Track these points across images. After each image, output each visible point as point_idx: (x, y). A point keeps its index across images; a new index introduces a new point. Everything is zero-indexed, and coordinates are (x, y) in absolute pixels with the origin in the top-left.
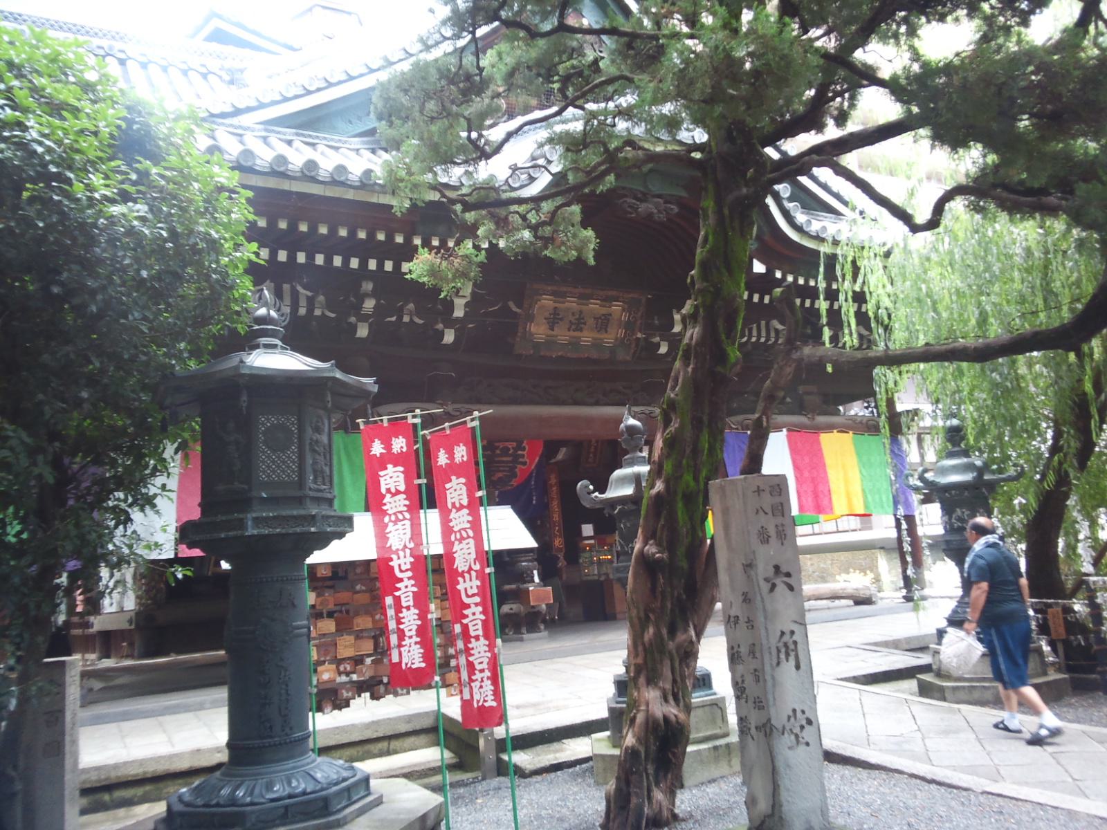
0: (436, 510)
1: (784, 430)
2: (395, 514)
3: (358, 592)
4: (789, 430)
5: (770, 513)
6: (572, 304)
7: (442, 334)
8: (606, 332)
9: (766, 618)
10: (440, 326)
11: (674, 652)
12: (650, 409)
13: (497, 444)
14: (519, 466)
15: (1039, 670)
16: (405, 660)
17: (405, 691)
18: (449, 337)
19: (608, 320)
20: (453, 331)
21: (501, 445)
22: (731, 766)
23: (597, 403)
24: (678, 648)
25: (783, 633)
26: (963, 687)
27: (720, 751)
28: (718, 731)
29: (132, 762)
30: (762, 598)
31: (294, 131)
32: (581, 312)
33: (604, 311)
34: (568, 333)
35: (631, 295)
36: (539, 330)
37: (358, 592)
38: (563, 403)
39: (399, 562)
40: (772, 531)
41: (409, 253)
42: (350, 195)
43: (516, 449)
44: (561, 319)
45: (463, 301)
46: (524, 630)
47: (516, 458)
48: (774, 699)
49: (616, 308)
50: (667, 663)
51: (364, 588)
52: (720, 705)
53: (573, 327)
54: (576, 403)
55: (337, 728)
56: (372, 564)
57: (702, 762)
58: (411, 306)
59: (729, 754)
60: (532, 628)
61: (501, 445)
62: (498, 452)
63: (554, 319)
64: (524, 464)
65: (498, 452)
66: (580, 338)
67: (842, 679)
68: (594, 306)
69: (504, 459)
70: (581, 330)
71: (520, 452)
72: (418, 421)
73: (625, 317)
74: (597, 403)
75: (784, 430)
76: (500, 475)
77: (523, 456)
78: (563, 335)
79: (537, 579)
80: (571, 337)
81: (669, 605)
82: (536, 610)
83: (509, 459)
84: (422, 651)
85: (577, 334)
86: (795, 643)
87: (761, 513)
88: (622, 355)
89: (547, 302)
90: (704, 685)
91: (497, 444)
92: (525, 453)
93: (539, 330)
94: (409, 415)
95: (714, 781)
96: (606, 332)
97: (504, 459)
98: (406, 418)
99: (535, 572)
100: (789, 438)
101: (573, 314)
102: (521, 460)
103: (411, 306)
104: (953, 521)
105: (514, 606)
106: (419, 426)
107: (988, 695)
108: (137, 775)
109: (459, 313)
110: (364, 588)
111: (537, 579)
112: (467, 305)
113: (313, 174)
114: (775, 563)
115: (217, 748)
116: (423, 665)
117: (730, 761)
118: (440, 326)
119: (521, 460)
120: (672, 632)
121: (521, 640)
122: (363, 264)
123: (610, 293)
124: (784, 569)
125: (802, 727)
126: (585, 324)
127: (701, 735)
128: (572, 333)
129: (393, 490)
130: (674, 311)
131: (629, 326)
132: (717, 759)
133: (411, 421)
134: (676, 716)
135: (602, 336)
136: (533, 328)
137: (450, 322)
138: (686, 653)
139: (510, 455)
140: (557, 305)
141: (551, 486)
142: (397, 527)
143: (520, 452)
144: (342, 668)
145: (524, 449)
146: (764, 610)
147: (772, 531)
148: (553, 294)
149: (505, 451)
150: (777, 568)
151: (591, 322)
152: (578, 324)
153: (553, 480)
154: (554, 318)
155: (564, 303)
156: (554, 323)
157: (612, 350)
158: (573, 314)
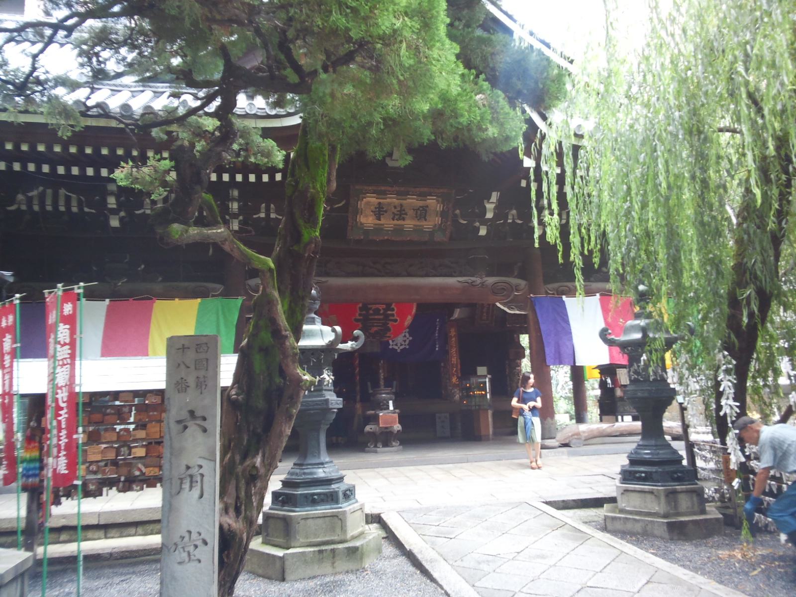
0: (46, 359)
1: (598, 295)
2: (62, 360)
3: (108, 414)
4: (601, 295)
5: (193, 367)
6: (392, 200)
7: (478, 230)
8: (426, 220)
9: (171, 454)
10: (477, 224)
11: (240, 474)
12: (473, 279)
13: (369, 306)
14: (390, 323)
15: (696, 508)
16: (58, 469)
17: (138, 488)
18: (483, 232)
19: (426, 211)
20: (486, 227)
21: (374, 307)
22: (334, 568)
23: (427, 275)
24: (244, 471)
25: (188, 468)
26: (620, 518)
27: (325, 554)
28: (336, 538)
29: (4, 519)
30: (171, 438)
31: (168, 85)
32: (401, 205)
33: (421, 203)
34: (392, 222)
35: (441, 191)
36: (367, 220)
37: (108, 414)
38: (398, 275)
39: (62, 395)
40: (191, 381)
41: (113, 163)
42: (114, 124)
43: (385, 310)
44: (386, 211)
45: (493, 206)
46: (380, 445)
47: (387, 317)
48: (168, 522)
49: (432, 202)
50: (233, 482)
51: (113, 412)
52: (340, 517)
53: (397, 217)
54: (410, 275)
55: (151, 508)
56: (121, 394)
57: (306, 562)
58: (514, 212)
59: (334, 557)
60: (386, 444)
61: (374, 307)
62: (371, 312)
63: (379, 212)
64: (396, 321)
65: (371, 312)
66: (403, 225)
67: (547, 503)
68: (412, 201)
69: (376, 317)
70: (404, 219)
71: (389, 312)
72: (81, 291)
73: (439, 208)
74: (427, 275)
75: (598, 295)
76: (375, 329)
77: (393, 315)
78: (388, 223)
79: (391, 408)
80: (414, 225)
81: (246, 437)
82: (388, 430)
83: (381, 317)
84: (66, 461)
85: (400, 222)
86: (202, 475)
87: (183, 366)
88: (439, 237)
89: (372, 200)
90: (332, 500)
91: (369, 306)
92: (394, 312)
93: (367, 220)
94: (76, 287)
95: (314, 577)
96: (426, 220)
97: (376, 317)
98: (73, 289)
99: (391, 402)
100: (602, 301)
101: (395, 207)
102: (391, 318)
103: (514, 212)
104: (632, 373)
105: (373, 427)
106: (82, 295)
107: (638, 527)
108: (7, 528)
109: (489, 215)
110: (113, 412)
111: (391, 408)
112: (495, 208)
113: (129, 114)
114: (190, 408)
115: (63, 515)
116: (66, 472)
117: (333, 563)
118: (477, 224)
119: (391, 318)
120: (244, 457)
121: (376, 452)
122: (233, 177)
123: (422, 190)
124: (198, 413)
125: (196, 547)
126: (406, 214)
127: (319, 540)
128: (396, 222)
129: (62, 343)
130: (485, 201)
131: (443, 214)
132: (321, 561)
133: (77, 291)
134: (229, 525)
135: (421, 224)
136: (362, 219)
137: (484, 222)
138: (251, 475)
139: (381, 315)
140: (381, 201)
141: (451, 337)
142: (62, 369)
143: (389, 312)
144: (91, 468)
145: (393, 310)
146: (171, 447)
147: (191, 381)
148: (398, 194)
149: (377, 311)
150: (192, 413)
151: (411, 213)
152: (401, 214)
153: (453, 332)
154: (379, 211)
155: (405, 199)
156: (380, 215)
157: (431, 234)
158: (395, 207)
